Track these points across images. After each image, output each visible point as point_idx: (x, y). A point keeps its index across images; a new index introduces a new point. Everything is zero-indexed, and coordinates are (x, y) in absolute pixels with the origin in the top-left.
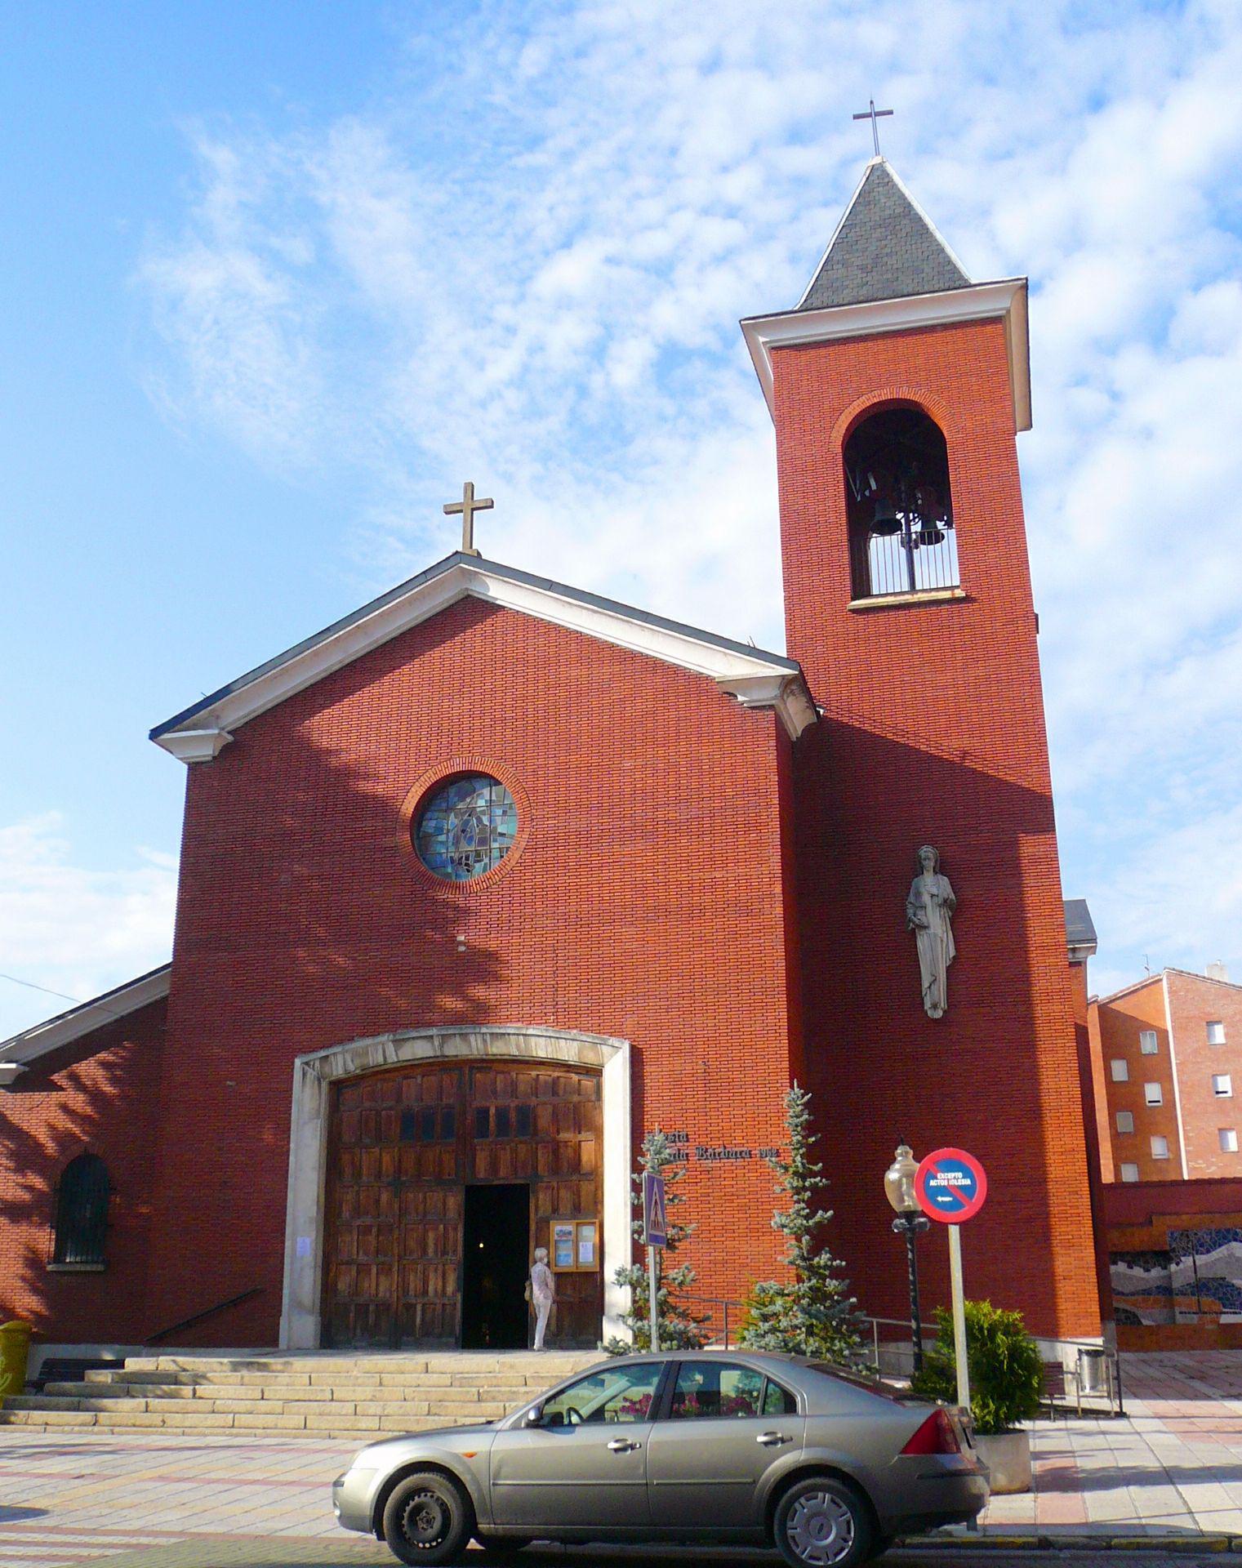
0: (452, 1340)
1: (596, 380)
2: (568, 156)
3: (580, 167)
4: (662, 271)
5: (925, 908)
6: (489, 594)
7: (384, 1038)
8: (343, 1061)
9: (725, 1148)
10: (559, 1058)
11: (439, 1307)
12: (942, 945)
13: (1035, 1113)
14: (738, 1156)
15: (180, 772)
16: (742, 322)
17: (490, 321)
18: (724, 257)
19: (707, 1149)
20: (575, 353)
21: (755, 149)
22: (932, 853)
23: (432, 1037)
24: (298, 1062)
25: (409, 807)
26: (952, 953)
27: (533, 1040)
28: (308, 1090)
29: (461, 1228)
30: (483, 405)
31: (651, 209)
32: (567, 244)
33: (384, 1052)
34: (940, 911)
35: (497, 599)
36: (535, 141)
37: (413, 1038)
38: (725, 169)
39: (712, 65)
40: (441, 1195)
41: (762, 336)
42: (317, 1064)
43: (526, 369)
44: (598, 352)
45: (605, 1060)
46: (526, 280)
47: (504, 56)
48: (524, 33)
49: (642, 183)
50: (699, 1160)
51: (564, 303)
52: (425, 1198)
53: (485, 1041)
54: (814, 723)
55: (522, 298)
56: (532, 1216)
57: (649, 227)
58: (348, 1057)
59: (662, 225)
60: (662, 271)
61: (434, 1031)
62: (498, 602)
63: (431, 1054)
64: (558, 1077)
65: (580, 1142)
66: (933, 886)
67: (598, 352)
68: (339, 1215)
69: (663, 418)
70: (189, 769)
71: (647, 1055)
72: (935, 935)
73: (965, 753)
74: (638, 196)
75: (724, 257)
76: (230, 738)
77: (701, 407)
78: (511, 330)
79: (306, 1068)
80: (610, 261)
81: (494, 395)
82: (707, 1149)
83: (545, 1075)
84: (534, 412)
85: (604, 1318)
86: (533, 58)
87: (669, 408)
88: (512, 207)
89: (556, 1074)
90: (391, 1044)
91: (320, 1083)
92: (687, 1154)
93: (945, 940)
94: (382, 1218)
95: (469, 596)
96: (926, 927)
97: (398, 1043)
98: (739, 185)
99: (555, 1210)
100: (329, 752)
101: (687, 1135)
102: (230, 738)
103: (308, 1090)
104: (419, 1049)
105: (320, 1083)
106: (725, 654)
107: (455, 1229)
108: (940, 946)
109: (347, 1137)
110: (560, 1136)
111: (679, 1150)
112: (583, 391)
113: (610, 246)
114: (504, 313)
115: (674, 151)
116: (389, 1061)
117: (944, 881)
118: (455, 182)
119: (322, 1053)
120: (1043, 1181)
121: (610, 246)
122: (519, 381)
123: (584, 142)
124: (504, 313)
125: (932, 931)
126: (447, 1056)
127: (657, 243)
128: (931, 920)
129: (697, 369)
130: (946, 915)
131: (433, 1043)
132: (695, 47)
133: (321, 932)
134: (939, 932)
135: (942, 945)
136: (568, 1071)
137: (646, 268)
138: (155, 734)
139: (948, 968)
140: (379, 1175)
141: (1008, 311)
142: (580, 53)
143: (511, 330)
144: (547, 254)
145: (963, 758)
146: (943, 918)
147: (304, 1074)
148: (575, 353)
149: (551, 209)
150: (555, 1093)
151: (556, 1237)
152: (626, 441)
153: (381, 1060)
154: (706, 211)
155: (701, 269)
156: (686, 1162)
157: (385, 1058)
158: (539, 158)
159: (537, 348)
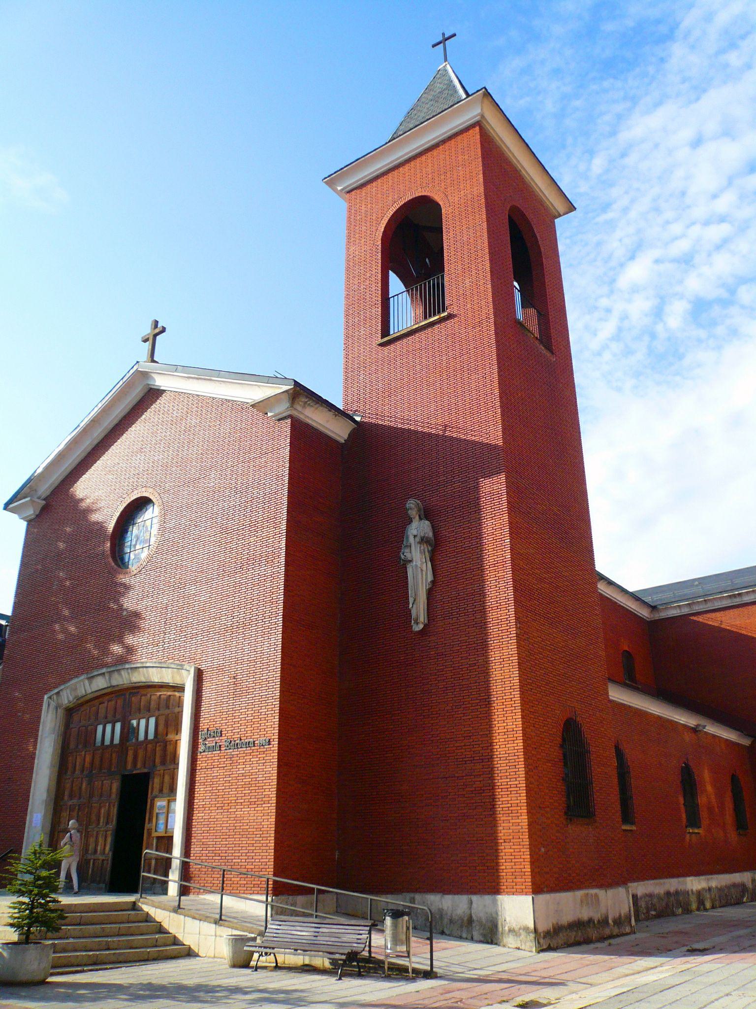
0: (104, 886)
1: (659, 328)
2: (626, 210)
3: (633, 214)
4: (687, 261)
5: (410, 546)
6: (156, 384)
7: (83, 677)
8: (67, 695)
9: (241, 740)
10: (165, 681)
11: (100, 862)
12: (422, 574)
13: (486, 702)
14: (247, 746)
15: (24, 525)
16: (324, 181)
17: (596, 308)
18: (722, 245)
19: (231, 741)
20: (646, 315)
21: (730, 181)
22: (413, 504)
23: (104, 674)
24: (46, 697)
25: (111, 526)
26: (430, 578)
27: (150, 669)
28: (50, 715)
29: (116, 806)
30: (599, 354)
31: (676, 228)
32: (632, 258)
33: (84, 686)
34: (420, 547)
35: (160, 386)
36: (606, 207)
37: (96, 675)
38: (715, 196)
39: (697, 143)
40: (109, 782)
41: (340, 186)
42: (55, 696)
43: (620, 329)
44: (658, 313)
45: (185, 681)
46: (613, 281)
47: (582, 167)
48: (591, 153)
49: (669, 215)
50: (226, 749)
51: (635, 289)
52: (102, 785)
53: (129, 673)
54: (354, 429)
55: (612, 292)
56: (149, 796)
57: (676, 238)
58: (68, 691)
59: (683, 236)
60: (687, 261)
61: (104, 670)
62: (162, 388)
63: (105, 686)
64: (170, 696)
65: (177, 740)
66: (419, 528)
67: (658, 313)
68: (63, 799)
69: (700, 341)
70: (28, 525)
71: (205, 675)
72: (416, 566)
73: (446, 426)
74: (668, 222)
75: (722, 245)
76: (44, 502)
77: (720, 330)
78: (608, 310)
79: (50, 701)
80: (657, 261)
81: (605, 347)
82: (231, 741)
83: (165, 693)
84: (628, 352)
85: (170, 870)
86: (598, 164)
87: (702, 333)
88: (599, 244)
89: (169, 693)
90: (87, 682)
91: (57, 710)
92: (220, 746)
93: (424, 569)
94: (82, 800)
95: (151, 389)
96: (411, 561)
97: (90, 679)
98: (723, 204)
99: (161, 791)
100: (82, 500)
101: (221, 731)
102: (44, 502)
103: (50, 715)
104: (100, 683)
105: (57, 710)
106: (259, 386)
107: (114, 806)
108: (420, 575)
109: (72, 745)
110: (168, 737)
111: (216, 743)
112: (653, 336)
113: (656, 253)
114: (604, 302)
115: (683, 194)
116: (88, 692)
117: (426, 523)
118: (566, 238)
119: (56, 691)
120: (490, 758)
121: (656, 253)
122: (617, 337)
123: (633, 201)
124: (604, 302)
125: (414, 563)
126: (114, 686)
127: (682, 247)
128: (414, 556)
129: (716, 310)
130: (426, 550)
131: (105, 679)
132: (687, 134)
133: (66, 612)
134: (419, 564)
135: (422, 574)
136: (174, 691)
137: (676, 261)
138: (6, 507)
139: (430, 592)
140: (82, 771)
141: (483, 116)
142: (623, 155)
143: (608, 310)
144: (622, 265)
145: (445, 431)
146: (422, 552)
147: (49, 705)
148: (646, 315)
149: (620, 240)
150: (168, 707)
151: (157, 811)
152: (681, 357)
153: (84, 692)
154: (707, 223)
155: (709, 255)
156: (219, 752)
157: (85, 691)
158: (609, 215)
159: (624, 317)
